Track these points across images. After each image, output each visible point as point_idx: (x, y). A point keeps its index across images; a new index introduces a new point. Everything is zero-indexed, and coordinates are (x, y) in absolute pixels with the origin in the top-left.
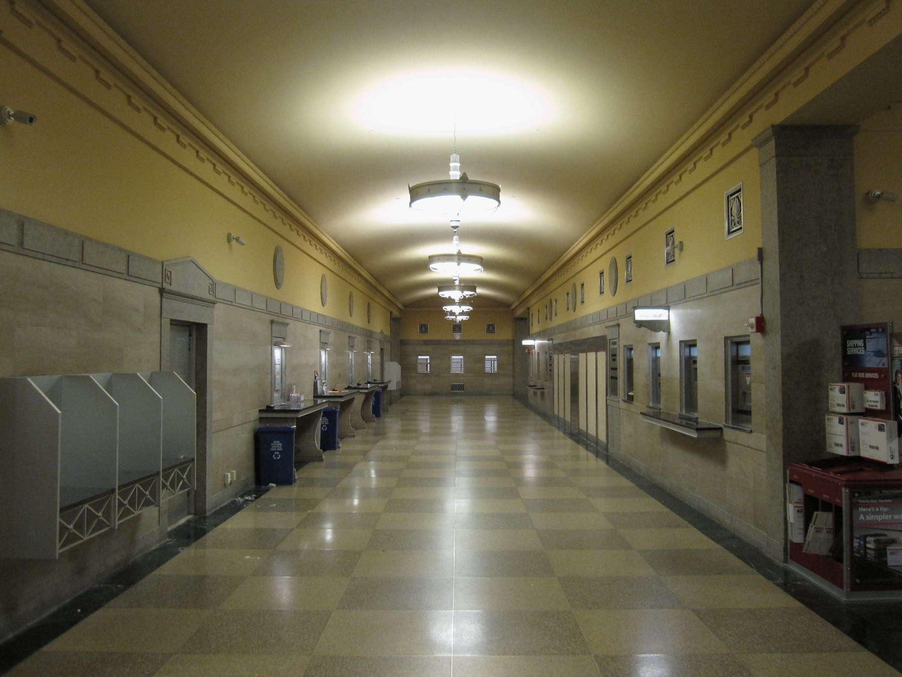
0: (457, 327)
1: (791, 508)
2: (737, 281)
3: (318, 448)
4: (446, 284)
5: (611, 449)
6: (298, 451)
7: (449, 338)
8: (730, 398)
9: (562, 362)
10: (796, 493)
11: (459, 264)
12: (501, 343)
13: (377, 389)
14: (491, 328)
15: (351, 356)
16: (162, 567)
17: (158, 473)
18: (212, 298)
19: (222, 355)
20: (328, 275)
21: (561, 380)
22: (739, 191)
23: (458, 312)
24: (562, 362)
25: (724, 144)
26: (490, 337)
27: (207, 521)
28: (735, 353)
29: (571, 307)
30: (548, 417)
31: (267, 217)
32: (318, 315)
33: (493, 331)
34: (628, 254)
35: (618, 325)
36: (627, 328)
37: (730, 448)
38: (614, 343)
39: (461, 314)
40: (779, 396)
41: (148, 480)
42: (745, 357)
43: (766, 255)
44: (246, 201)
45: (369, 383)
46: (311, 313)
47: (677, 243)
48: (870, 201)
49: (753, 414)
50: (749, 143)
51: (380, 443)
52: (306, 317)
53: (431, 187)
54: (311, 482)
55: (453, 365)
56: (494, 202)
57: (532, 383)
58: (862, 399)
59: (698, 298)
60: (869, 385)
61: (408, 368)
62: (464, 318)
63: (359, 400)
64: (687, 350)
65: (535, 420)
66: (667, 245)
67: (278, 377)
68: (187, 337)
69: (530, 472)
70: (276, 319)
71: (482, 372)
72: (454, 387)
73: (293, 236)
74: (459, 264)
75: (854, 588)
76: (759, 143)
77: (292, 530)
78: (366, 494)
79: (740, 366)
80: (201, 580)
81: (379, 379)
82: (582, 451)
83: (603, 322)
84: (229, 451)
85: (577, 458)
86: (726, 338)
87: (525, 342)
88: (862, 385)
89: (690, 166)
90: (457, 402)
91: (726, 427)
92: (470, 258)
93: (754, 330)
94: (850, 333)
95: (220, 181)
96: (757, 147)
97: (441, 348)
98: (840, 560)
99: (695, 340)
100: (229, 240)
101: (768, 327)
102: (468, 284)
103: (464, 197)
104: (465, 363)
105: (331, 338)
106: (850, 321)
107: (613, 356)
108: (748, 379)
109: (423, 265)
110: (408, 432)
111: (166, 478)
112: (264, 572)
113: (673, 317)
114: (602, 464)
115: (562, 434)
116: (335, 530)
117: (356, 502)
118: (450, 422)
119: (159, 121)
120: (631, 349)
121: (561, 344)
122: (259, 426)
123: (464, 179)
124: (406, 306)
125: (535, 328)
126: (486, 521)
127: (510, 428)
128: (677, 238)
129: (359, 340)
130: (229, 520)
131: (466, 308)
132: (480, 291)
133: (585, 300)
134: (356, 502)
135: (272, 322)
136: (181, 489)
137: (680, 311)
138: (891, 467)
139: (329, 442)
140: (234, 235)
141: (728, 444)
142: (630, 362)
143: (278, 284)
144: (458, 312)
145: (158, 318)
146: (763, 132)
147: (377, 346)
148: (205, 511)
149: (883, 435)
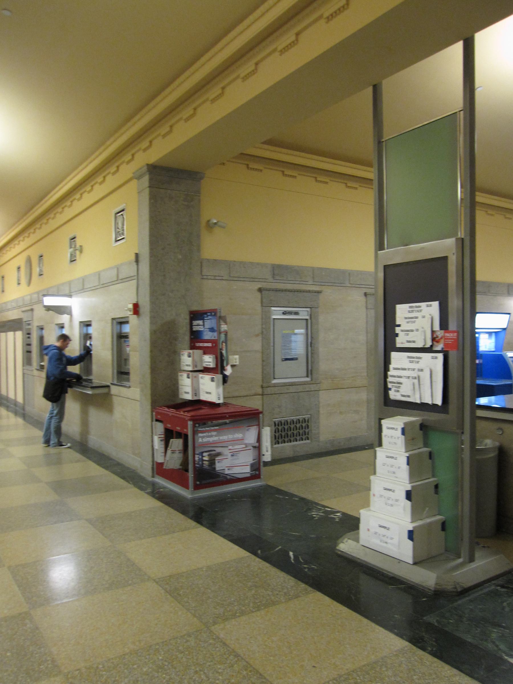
1: (156, 439)
2: (121, 277)
10: (160, 428)
22: (123, 210)
34: (40, 254)
35: (32, 310)
36: (39, 312)
37: (116, 400)
38: (29, 324)
40: (148, 360)
43: (140, 259)
47: (78, 246)
48: (210, 226)
50: (131, 175)
58: (202, 361)
59: (94, 289)
60: (206, 351)
64: (85, 328)
75: (197, 487)
79: (123, 340)
83: (19, 307)
88: (200, 352)
91: (112, 384)
93: (132, 313)
94: (196, 315)
96: (136, 179)
98: (187, 470)
99: (90, 321)
101: (141, 310)
106: (195, 308)
108: (128, 349)
114: (20, 421)
128: (79, 242)
138: (218, 405)
141: (114, 398)
146: (140, 169)
149: (214, 384)
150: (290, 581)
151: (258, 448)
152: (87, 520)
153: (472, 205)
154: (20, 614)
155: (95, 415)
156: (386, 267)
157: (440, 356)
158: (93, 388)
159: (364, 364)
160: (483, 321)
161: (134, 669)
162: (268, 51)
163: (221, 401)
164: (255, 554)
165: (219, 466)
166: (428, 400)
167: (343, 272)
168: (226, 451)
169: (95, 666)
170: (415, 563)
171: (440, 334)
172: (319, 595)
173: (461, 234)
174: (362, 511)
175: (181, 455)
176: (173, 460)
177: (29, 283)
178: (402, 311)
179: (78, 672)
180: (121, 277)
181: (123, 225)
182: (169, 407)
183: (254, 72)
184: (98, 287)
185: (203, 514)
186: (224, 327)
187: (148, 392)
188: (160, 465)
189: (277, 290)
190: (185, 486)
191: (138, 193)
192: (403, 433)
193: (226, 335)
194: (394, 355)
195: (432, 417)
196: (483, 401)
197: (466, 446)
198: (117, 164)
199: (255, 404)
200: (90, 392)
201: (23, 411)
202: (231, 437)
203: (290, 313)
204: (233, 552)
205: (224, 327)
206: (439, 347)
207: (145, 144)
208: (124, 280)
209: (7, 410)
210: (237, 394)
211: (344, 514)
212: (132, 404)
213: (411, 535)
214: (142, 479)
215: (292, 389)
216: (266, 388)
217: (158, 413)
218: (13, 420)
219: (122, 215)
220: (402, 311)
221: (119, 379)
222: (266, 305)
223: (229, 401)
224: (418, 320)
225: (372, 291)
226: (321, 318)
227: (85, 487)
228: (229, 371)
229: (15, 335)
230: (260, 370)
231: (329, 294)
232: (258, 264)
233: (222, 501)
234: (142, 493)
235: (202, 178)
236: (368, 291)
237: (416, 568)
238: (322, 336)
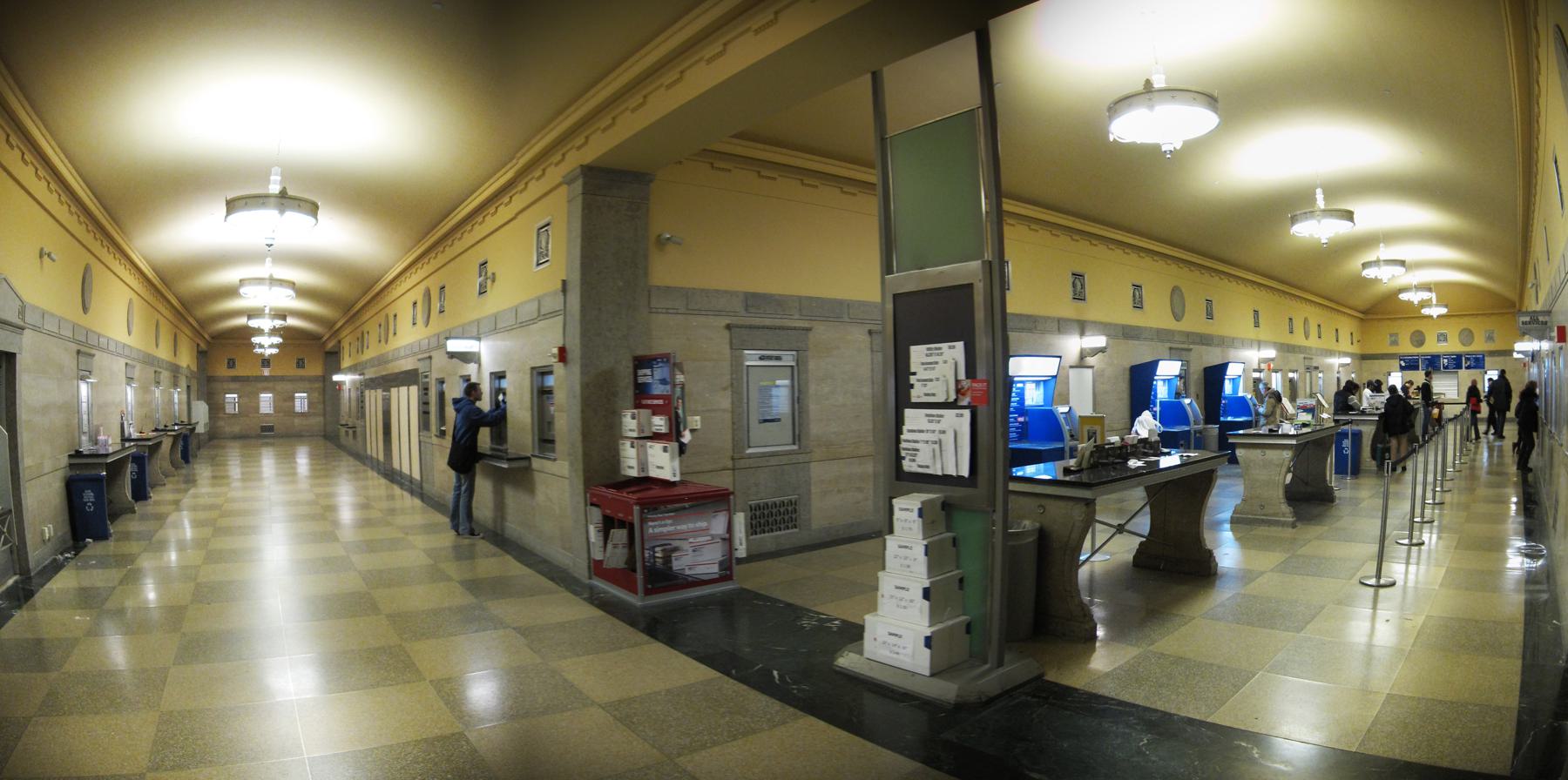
0: (266, 362)
1: (592, 529)
4: (252, 314)
6: (110, 502)
10: (596, 514)
12: (311, 380)
15: (157, 393)
23: (267, 344)
24: (374, 398)
26: (301, 372)
30: (361, 457)
31: (79, 230)
36: (439, 360)
37: (538, 477)
39: (272, 346)
40: (579, 424)
43: (569, 287)
44: (61, 212)
48: (661, 243)
50: (560, 180)
52: (112, 348)
54: (126, 536)
55: (262, 404)
56: (311, 219)
58: (650, 424)
60: (656, 411)
61: (216, 409)
62: (275, 351)
65: (347, 462)
67: (85, 417)
70: (83, 349)
71: (291, 412)
72: (264, 429)
73: (103, 253)
75: (648, 592)
76: (568, 181)
78: (182, 546)
82: (397, 490)
83: (415, 354)
84: (42, 498)
85: (391, 497)
87: (336, 378)
88: (648, 411)
90: (267, 444)
94: (642, 362)
95: (40, 188)
98: (634, 571)
100: (41, 256)
102: (282, 315)
103: (282, 212)
106: (640, 352)
107: (425, 390)
109: (231, 292)
110: (219, 478)
112: (94, 632)
114: (417, 502)
116: (157, 590)
121: (372, 380)
123: (283, 194)
125: (346, 363)
127: (323, 469)
128: (490, 269)
129: (165, 375)
131: (277, 340)
132: (292, 322)
135: (79, 352)
138: (674, 484)
139: (140, 493)
140: (46, 250)
141: (536, 474)
142: (441, 395)
143: (85, 309)
144: (267, 344)
147: (183, 383)
148: (29, 571)
149: (667, 455)
150: (775, 706)
151: (728, 540)
153: (999, 216)
155: (512, 496)
156: (895, 296)
157: (967, 413)
158: (509, 460)
159: (870, 426)
160: (1020, 367)
162: (740, 30)
163: (677, 479)
164: (728, 674)
165: (677, 565)
166: (951, 471)
167: (841, 302)
168: (685, 545)
170: (932, 675)
171: (966, 384)
172: (812, 720)
173: (988, 256)
174: (867, 617)
175: (626, 551)
176: (615, 557)
178: (918, 353)
180: (543, 311)
182: (608, 486)
183: (721, 54)
185: (658, 627)
186: (680, 378)
187: (580, 466)
188: (598, 563)
189: (751, 327)
190: (633, 590)
192: (920, 515)
193: (683, 388)
194: (909, 413)
195: (958, 493)
196: (1030, 470)
197: (998, 528)
199: (724, 481)
202: (691, 526)
203: (769, 358)
204: (698, 673)
205: (680, 378)
206: (965, 401)
207: (580, 141)
210: (698, 468)
211: (843, 621)
212: (558, 485)
213: (928, 642)
214: (576, 581)
215: (773, 461)
216: (738, 459)
217: (593, 495)
218: (409, 501)
220: (918, 353)
221: (542, 450)
222: (737, 347)
223: (688, 478)
224: (937, 366)
225: (879, 328)
226: (812, 365)
227: (497, 588)
228: (687, 437)
230: (729, 437)
231: (821, 332)
232: (726, 292)
233: (684, 609)
235: (651, 181)
236: (874, 328)
237: (935, 680)
238: (812, 388)
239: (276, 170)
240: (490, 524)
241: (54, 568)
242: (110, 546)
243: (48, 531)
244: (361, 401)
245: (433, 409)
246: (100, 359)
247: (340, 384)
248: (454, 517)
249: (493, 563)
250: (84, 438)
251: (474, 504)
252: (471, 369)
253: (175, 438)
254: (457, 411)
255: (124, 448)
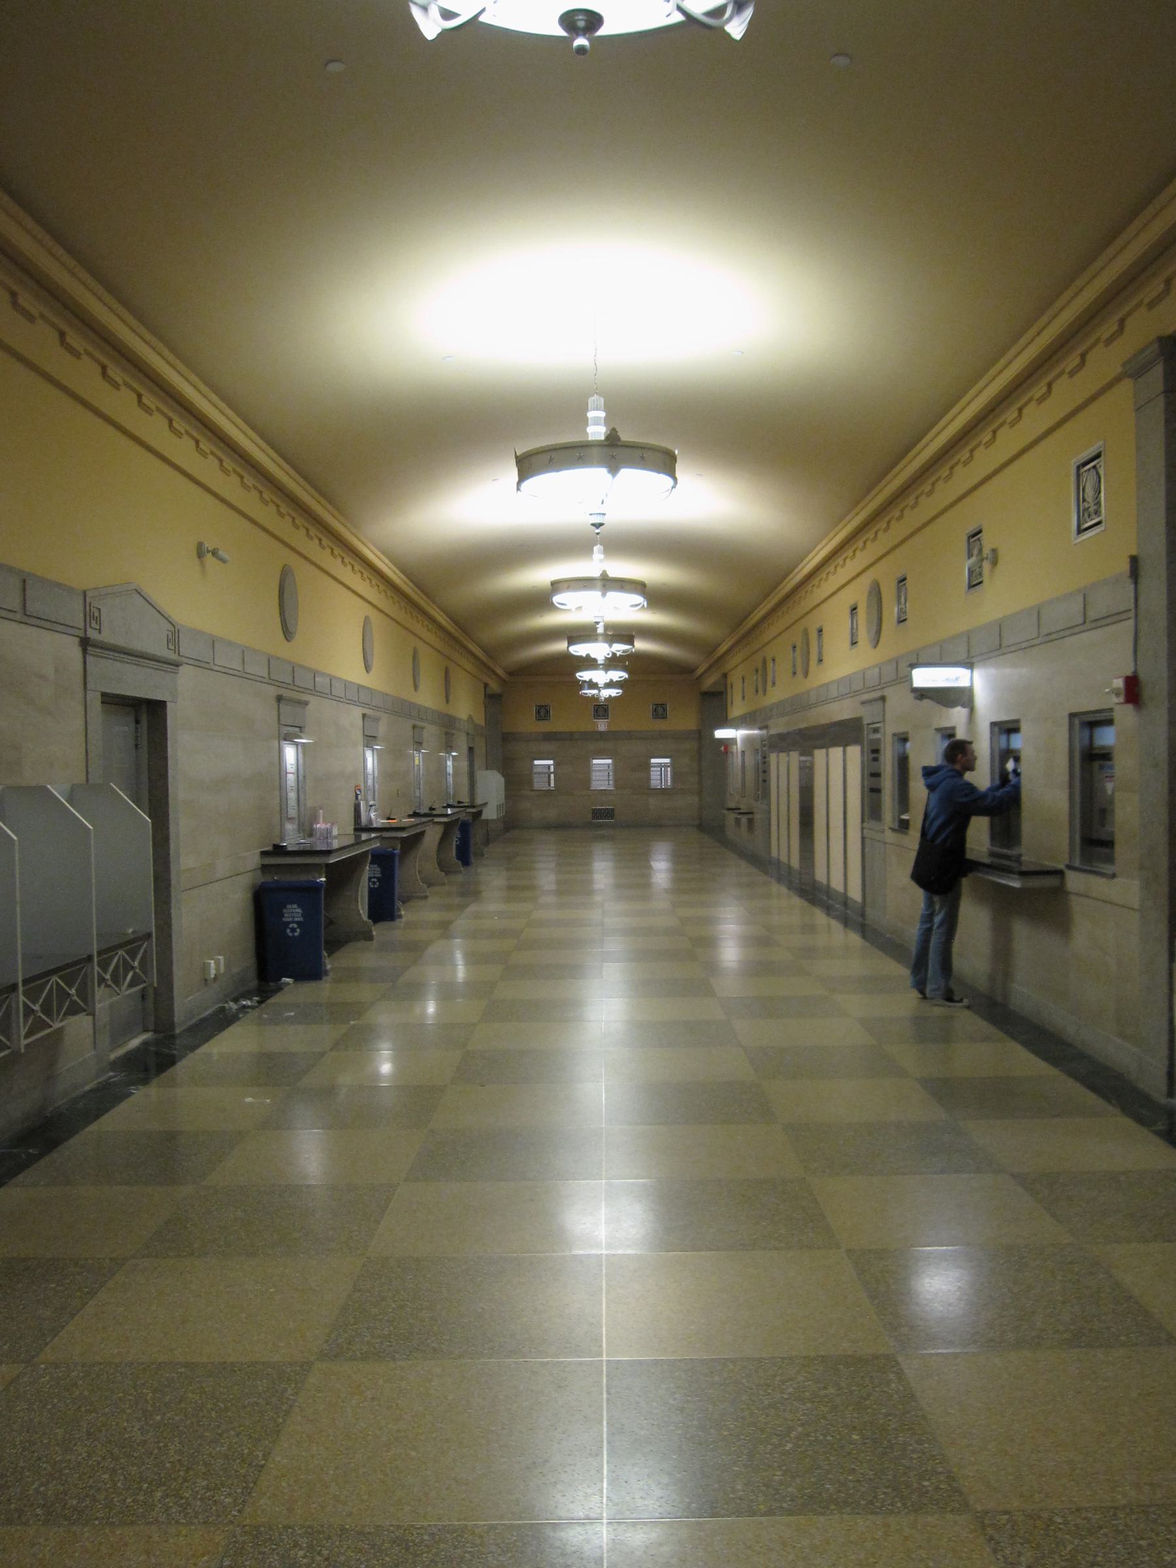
0: (601, 709)
2: (1092, 615)
3: (365, 917)
4: (584, 633)
5: (869, 911)
6: (331, 922)
7: (589, 728)
8: (1078, 821)
9: (785, 768)
11: (604, 595)
12: (678, 737)
13: (463, 817)
14: (660, 710)
16: (106, 1118)
17: (90, 958)
18: (173, 656)
19: (191, 756)
20: (376, 618)
21: (783, 799)
22: (1098, 456)
23: (603, 682)
24: (785, 768)
25: (1072, 374)
27: (178, 1041)
28: (1086, 742)
29: (799, 670)
30: (762, 862)
31: (265, 514)
32: (360, 687)
33: (664, 717)
34: (900, 575)
35: (883, 699)
36: (898, 700)
37: (1077, 906)
38: (876, 731)
41: (73, 970)
42: (1103, 748)
44: (230, 487)
45: (449, 806)
46: (347, 684)
47: (986, 551)
49: (1118, 847)
50: (1119, 370)
51: (472, 908)
52: (338, 690)
53: (554, 455)
54: (354, 975)
55: (595, 776)
56: (666, 480)
57: (732, 805)
59: (1025, 647)
61: (517, 781)
62: (614, 692)
63: (433, 835)
64: (1004, 738)
66: (970, 555)
67: (292, 795)
68: (133, 726)
69: (730, 954)
71: (644, 788)
72: (597, 814)
73: (311, 548)
74: (604, 595)
76: (1135, 371)
77: (322, 1054)
78: (447, 993)
79: (1096, 764)
80: (171, 1137)
81: (466, 800)
83: (856, 693)
84: (210, 923)
86: (1072, 716)
87: (720, 734)
89: (1011, 414)
90: (603, 838)
91: (1069, 867)
92: (623, 584)
93: (1122, 699)
95: (182, 450)
96: (1131, 376)
97: (574, 746)
99: (1017, 721)
100: (200, 552)
101: (1146, 693)
102: (622, 633)
103: (588, 655)
104: (615, 771)
105: (382, 729)
108: (1109, 786)
109: (541, 600)
110: (519, 890)
111: (104, 965)
113: (977, 681)
114: (855, 938)
115: (784, 890)
116: (395, 1060)
117: (431, 1008)
118: (590, 872)
119: (68, 339)
120: (904, 740)
121: (782, 737)
122: (261, 879)
123: (612, 440)
124: (511, 674)
125: (737, 708)
126: (652, 1034)
127: (693, 880)
128: (988, 542)
129: (431, 732)
130: (213, 1042)
131: (617, 675)
132: (641, 645)
133: (825, 658)
134: (431, 1008)
135: (279, 699)
136: (131, 985)
137: (992, 671)
139: (383, 908)
140: (208, 545)
141: (1073, 897)
142: (903, 762)
143: (288, 634)
144: (603, 682)
145: (79, 689)
146: (1143, 350)
147: (462, 743)
148: (172, 1025)
152: (1013, 1176)
154: (876, 1357)
155: (1026, 937)
158: (1024, 874)
161: (1140, 1547)
169: (1045, 1515)
177: (876, 642)
179: (1007, 1517)
180: (1092, 615)
181: (1098, 491)
184: (1036, 641)
191: (1137, 410)
198: (1080, 351)
200: (1016, 884)
201: (861, 919)
208: (1099, 623)
209: (828, 914)
218: (837, 935)
219: (1094, 467)
221: (1087, 858)
227: (997, 1098)
229: (844, 752)
234: (1143, 1132)
239: (593, 400)
240: (982, 984)
241: (221, 1021)
242: (323, 990)
243: (215, 966)
244: (763, 771)
245: (888, 784)
246: (317, 708)
247: (727, 743)
248: (919, 966)
249: (980, 1052)
250: (290, 827)
251: (956, 947)
252: (957, 717)
253: (448, 827)
254: (931, 787)
255: (358, 842)
